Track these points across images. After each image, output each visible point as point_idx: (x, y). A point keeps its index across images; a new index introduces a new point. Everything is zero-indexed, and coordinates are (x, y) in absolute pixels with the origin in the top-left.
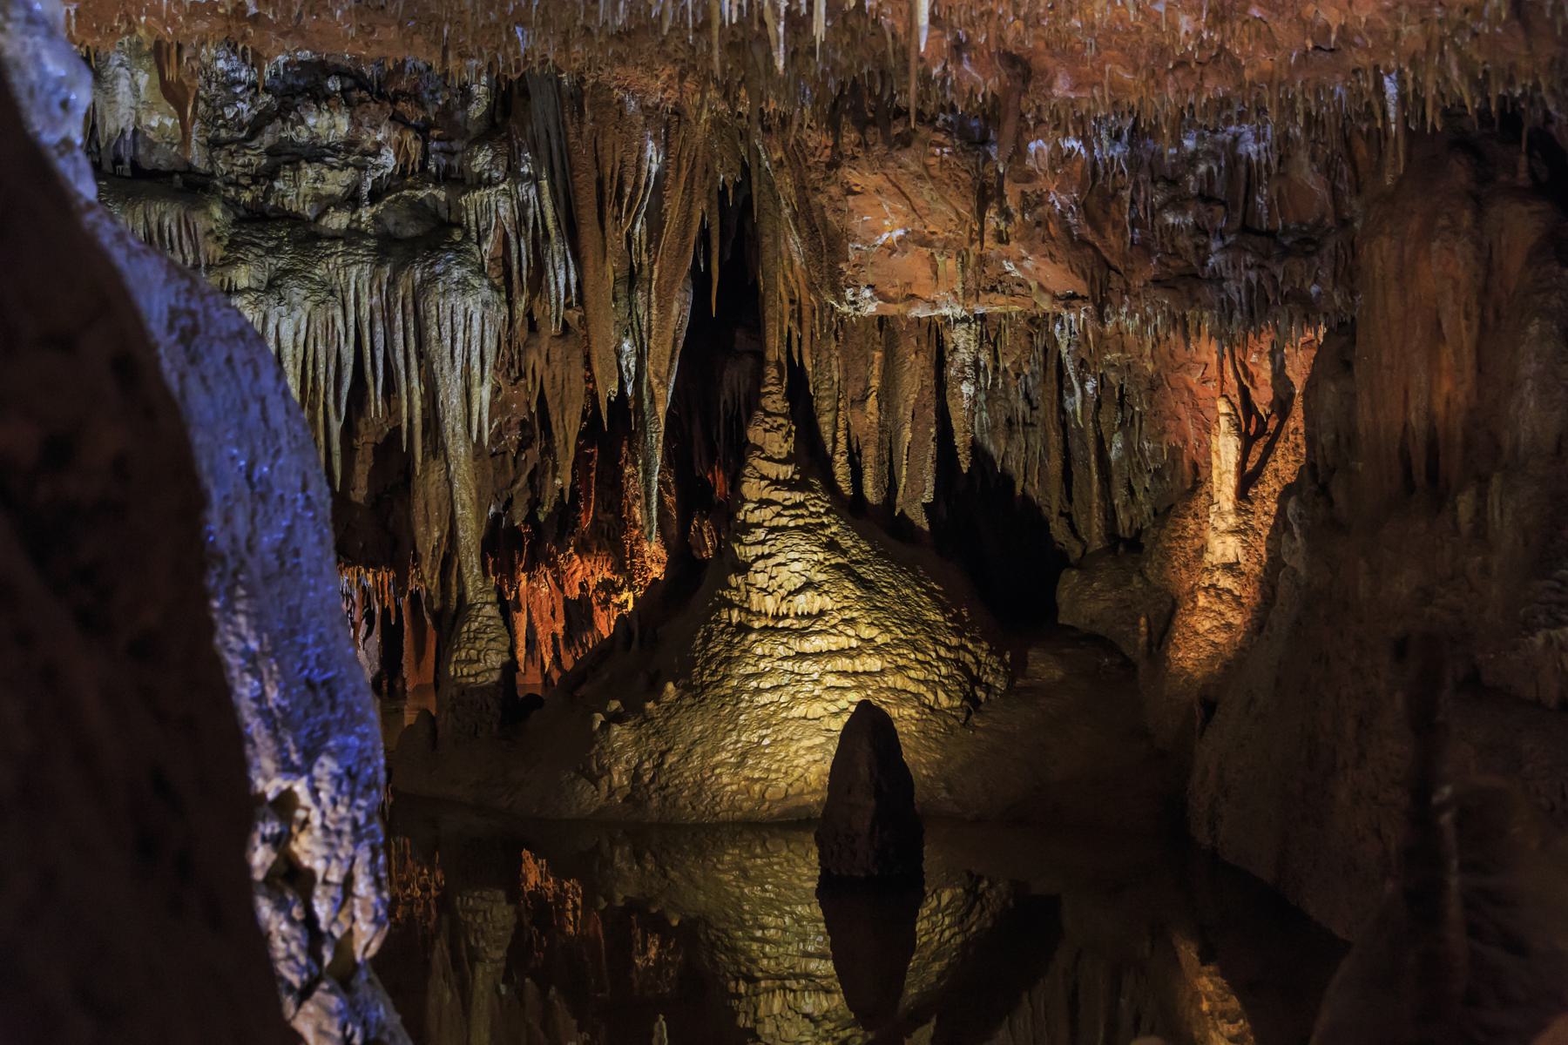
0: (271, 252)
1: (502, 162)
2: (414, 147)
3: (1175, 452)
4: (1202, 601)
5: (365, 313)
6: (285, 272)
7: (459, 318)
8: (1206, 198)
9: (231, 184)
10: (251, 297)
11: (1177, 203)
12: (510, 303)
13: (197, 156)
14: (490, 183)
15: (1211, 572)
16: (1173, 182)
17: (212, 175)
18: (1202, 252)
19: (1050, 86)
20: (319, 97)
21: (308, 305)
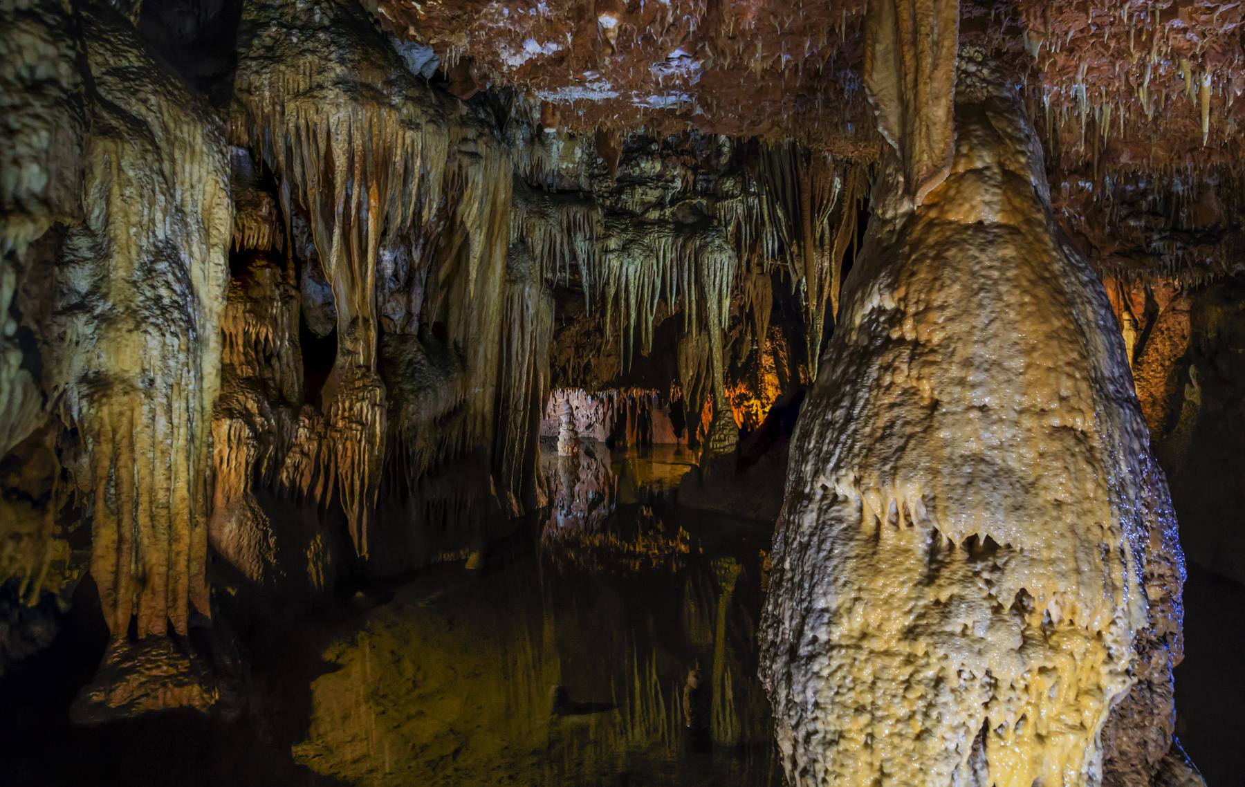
0: (624, 231)
1: (739, 186)
2: (691, 177)
5: (668, 262)
6: (631, 241)
7: (718, 265)
8: (1153, 212)
9: (599, 196)
11: (1137, 215)
12: (740, 259)
13: (584, 182)
14: (733, 196)
16: (1131, 204)
17: (591, 192)
19: (1118, 157)
20: (650, 155)
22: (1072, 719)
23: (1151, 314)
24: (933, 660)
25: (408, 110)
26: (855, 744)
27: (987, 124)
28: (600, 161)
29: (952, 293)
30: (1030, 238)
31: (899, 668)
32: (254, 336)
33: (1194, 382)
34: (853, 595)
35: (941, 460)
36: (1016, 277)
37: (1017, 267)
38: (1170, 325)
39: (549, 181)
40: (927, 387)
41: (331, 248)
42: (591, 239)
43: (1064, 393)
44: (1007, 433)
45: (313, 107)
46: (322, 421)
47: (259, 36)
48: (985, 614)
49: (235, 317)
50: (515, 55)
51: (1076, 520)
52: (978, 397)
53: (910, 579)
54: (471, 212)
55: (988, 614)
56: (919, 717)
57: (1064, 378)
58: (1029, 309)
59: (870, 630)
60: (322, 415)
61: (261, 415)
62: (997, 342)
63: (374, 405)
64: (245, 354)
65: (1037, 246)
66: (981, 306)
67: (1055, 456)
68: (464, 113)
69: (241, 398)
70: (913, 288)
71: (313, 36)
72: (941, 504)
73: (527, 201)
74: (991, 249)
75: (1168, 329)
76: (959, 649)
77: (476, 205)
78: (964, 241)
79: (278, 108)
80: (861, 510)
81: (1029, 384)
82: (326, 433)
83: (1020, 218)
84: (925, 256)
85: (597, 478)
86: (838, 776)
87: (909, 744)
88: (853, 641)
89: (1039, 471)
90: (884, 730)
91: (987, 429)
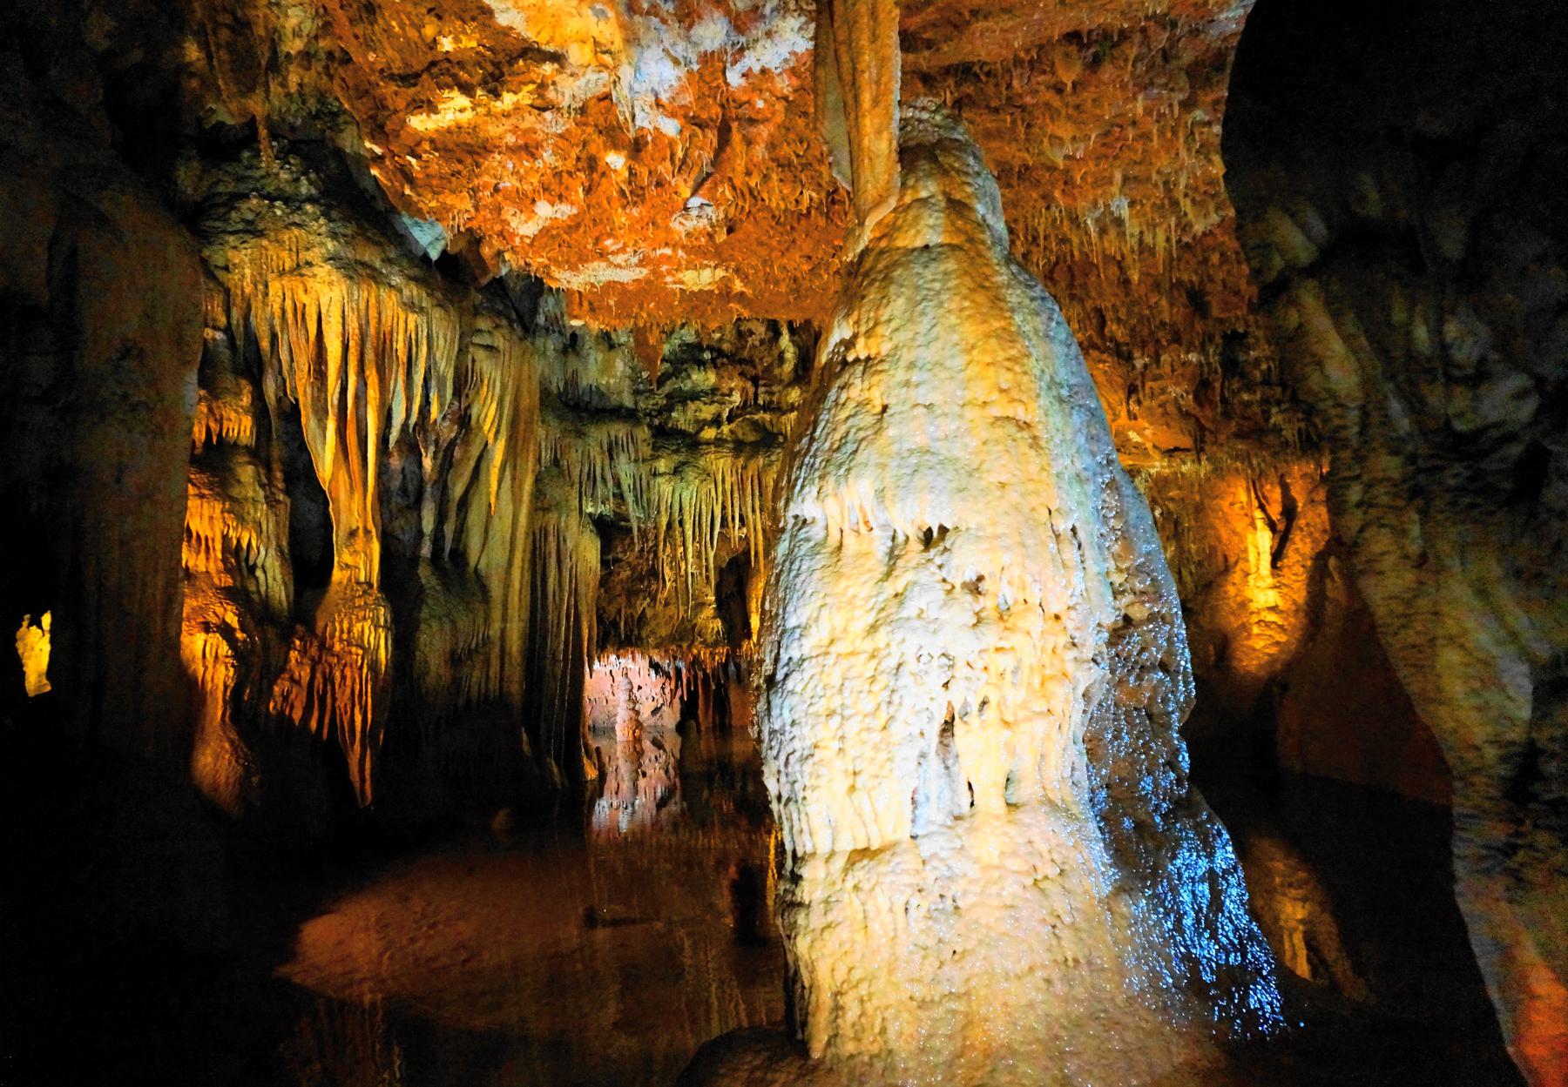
0: (676, 452)
3: (1213, 549)
4: (1256, 630)
5: (728, 487)
6: (683, 464)
8: (1266, 382)
10: (667, 477)
15: (1258, 613)
18: (1266, 415)
20: (701, 363)
21: (697, 482)
22: (1040, 706)
23: (1289, 512)
24: (893, 648)
25: (413, 291)
26: (827, 753)
27: (934, 159)
28: (645, 375)
29: (898, 305)
30: (972, 254)
31: (865, 664)
32: (235, 542)
33: (1336, 576)
34: (819, 603)
35: (890, 456)
36: (957, 286)
37: (958, 277)
38: (1309, 520)
39: (587, 399)
40: (878, 394)
41: (324, 442)
42: (636, 461)
43: (1004, 386)
44: (951, 426)
45: (301, 286)
46: (316, 643)
47: (238, 209)
48: (939, 593)
49: (211, 518)
50: (526, 222)
51: (1020, 500)
52: (923, 395)
53: (871, 578)
54: (488, 413)
55: (942, 595)
56: (884, 707)
57: (1003, 370)
58: (968, 313)
59: (837, 634)
60: (316, 636)
61: (243, 630)
62: (938, 345)
63: (377, 626)
64: (224, 560)
65: (979, 261)
66: (923, 314)
67: (997, 442)
68: (477, 302)
69: (219, 610)
70: (864, 309)
71: (300, 208)
72: (888, 493)
73: (561, 418)
74: (933, 265)
75: (1307, 525)
76: (915, 630)
77: (494, 406)
78: (910, 262)
79: (261, 287)
80: (827, 528)
81: (970, 380)
82: (320, 657)
83: (963, 238)
84: (874, 280)
85: (667, 772)
86: (814, 788)
87: (876, 736)
88: (823, 650)
89: (982, 457)
90: (852, 727)
91: (931, 423)
